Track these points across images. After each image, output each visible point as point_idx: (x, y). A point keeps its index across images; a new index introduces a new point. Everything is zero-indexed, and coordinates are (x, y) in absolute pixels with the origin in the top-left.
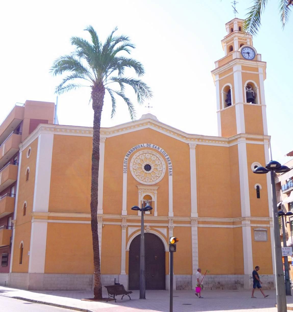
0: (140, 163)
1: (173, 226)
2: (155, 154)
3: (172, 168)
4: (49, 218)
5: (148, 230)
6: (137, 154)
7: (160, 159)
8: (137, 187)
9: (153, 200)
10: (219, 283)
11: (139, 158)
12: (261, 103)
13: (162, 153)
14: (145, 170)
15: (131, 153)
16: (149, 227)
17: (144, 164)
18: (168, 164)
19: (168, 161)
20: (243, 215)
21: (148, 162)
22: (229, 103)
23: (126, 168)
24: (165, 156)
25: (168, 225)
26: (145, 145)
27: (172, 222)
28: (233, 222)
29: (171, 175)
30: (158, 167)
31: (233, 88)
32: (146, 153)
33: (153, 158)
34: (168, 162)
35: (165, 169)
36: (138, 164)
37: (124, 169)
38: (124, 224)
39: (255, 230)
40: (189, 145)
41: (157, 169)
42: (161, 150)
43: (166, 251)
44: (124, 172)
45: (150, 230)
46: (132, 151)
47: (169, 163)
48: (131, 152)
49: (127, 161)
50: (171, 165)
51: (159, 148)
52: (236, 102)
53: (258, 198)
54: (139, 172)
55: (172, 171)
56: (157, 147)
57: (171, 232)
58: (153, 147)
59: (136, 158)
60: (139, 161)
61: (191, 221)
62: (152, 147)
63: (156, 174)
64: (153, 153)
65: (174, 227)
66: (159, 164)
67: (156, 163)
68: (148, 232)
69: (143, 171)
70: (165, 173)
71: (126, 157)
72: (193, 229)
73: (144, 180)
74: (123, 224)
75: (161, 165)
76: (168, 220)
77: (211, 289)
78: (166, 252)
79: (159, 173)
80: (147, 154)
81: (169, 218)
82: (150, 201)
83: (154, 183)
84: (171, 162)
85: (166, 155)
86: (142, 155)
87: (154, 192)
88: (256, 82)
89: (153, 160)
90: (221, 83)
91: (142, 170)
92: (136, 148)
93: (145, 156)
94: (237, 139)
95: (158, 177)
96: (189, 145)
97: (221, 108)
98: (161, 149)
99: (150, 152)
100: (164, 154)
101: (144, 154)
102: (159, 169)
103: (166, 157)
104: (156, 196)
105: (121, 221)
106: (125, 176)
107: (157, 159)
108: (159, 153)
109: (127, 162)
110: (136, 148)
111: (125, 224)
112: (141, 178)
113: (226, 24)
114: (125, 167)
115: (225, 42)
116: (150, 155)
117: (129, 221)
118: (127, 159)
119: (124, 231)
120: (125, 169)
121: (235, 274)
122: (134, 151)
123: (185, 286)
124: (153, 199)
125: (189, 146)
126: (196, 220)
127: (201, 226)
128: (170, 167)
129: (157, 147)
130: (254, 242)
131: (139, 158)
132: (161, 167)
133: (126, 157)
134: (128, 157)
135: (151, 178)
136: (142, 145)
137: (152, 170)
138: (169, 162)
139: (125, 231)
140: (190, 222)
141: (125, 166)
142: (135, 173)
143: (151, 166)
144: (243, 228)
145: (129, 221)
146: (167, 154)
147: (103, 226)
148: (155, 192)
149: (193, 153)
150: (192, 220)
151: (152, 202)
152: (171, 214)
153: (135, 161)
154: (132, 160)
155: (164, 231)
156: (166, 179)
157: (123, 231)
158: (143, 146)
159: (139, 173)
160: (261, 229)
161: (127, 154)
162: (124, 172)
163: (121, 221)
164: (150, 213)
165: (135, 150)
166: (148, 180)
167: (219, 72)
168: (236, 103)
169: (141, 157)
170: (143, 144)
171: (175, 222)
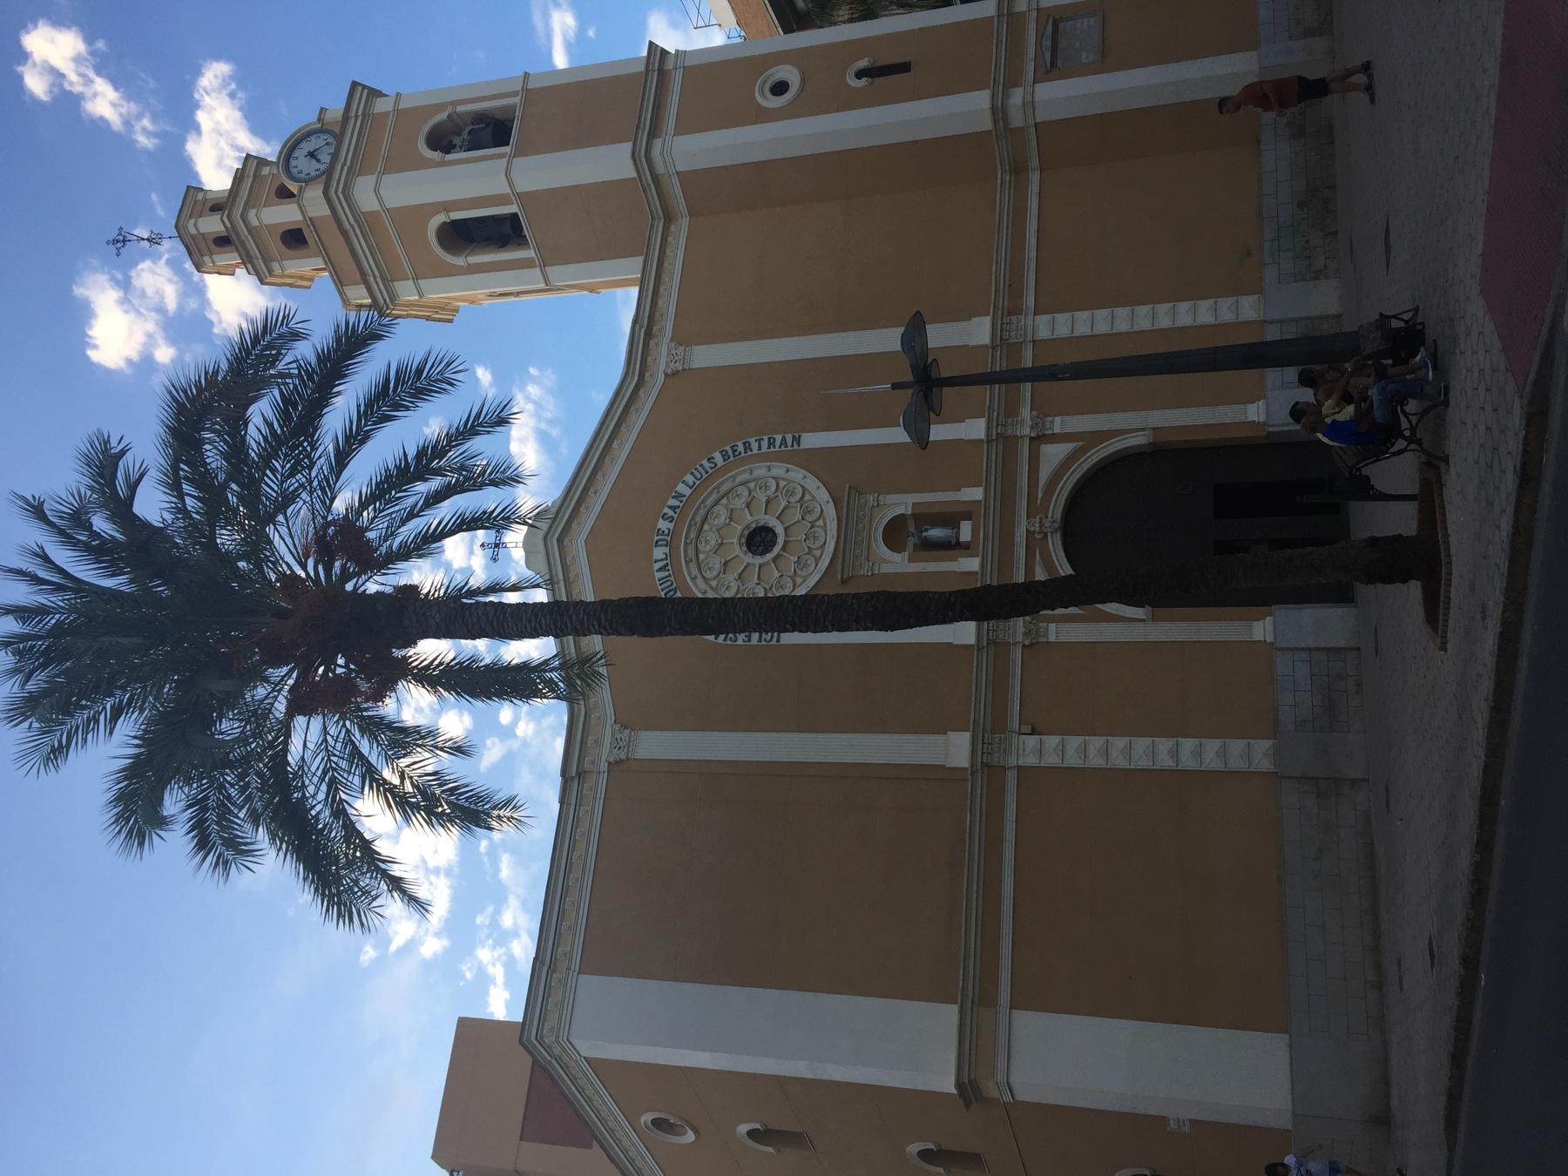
4: (987, 999)
10: (1301, 205)
12: (515, 94)
20: (986, 124)
22: (507, 229)
26: (659, 553)
29: (797, 440)
31: (446, 207)
39: (1053, 64)
41: (768, 502)
44: (774, 642)
50: (752, 440)
51: (678, 496)
53: (909, 70)
55: (779, 438)
57: (1058, 425)
62: (671, 526)
66: (746, 493)
73: (817, 553)
74: (1020, 638)
77: (1336, 233)
80: (708, 575)
82: (912, 528)
84: (740, 444)
93: (707, 553)
94: (656, 178)
98: (681, 488)
104: (890, 498)
107: (724, 501)
121: (1258, 142)
127: (1030, 301)
128: (765, 444)
130: (1105, 62)
136: (657, 566)
138: (741, 448)
139: (1052, 626)
144: (1041, 117)
146: (705, 462)
147: (1028, 729)
149: (706, 356)
155: (1053, 454)
156: (816, 462)
160: (1047, 43)
168: (377, 207)
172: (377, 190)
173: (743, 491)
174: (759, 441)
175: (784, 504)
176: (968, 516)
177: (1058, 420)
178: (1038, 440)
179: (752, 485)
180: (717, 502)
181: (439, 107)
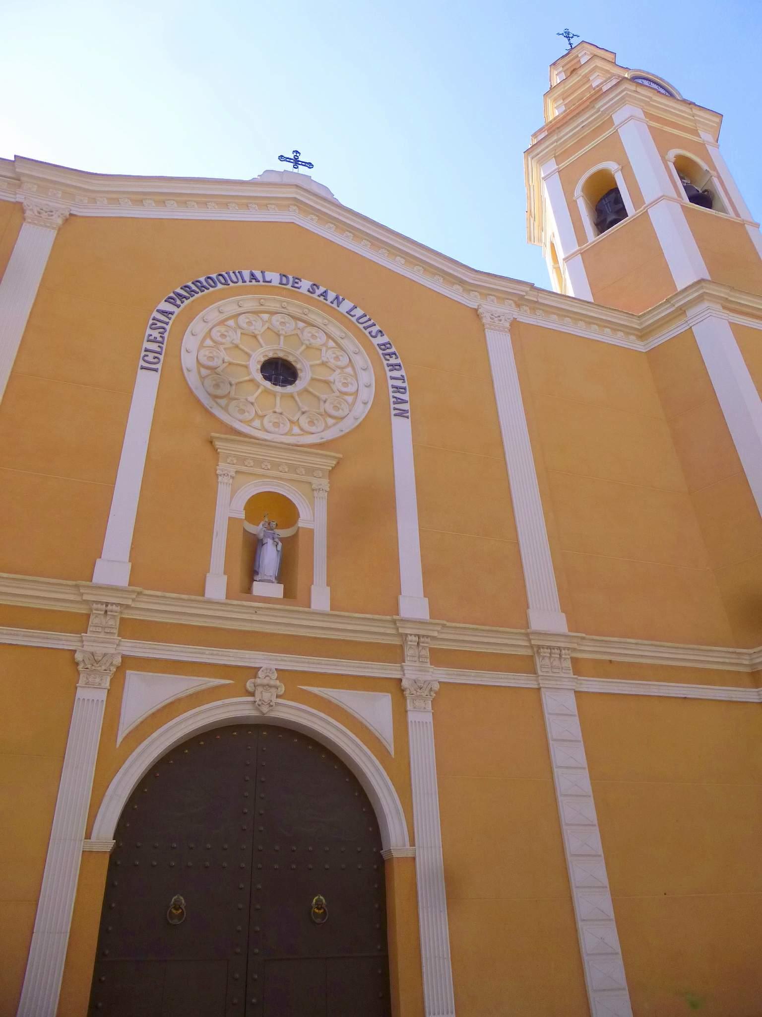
1: (429, 678)
2: (319, 321)
5: (266, 696)
7: (344, 343)
13: (354, 319)
14: (266, 378)
16: (276, 675)
19: (388, 357)
23: (159, 350)
25: (397, 675)
27: (426, 653)
28: (748, 670)
29: (402, 414)
31: (626, 168)
35: (368, 386)
36: (225, 349)
38: (99, 649)
42: (351, 310)
43: (395, 854)
44: (142, 363)
45: (280, 701)
47: (390, 362)
49: (167, 320)
52: (648, 198)
57: (421, 718)
58: (313, 293)
59: (222, 323)
60: (236, 338)
61: (531, 658)
63: (325, 402)
64: (312, 317)
65: (436, 687)
67: (324, 359)
68: (265, 709)
70: (369, 405)
72: (550, 701)
73: (257, 423)
74: (89, 647)
76: (397, 641)
78: (391, 859)
81: (401, 631)
85: (374, 329)
86: (251, 317)
87: (310, 483)
88: (703, 159)
90: (566, 178)
91: (249, 374)
94: (682, 311)
95: (330, 416)
97: (581, 238)
99: (292, 310)
102: (339, 386)
106: (146, 388)
107: (331, 344)
110: (223, 281)
111: (102, 644)
113: (554, 64)
115: (559, 96)
116: (296, 324)
119: (90, 698)
120: (151, 355)
126: (559, 648)
129: (331, 295)
132: (346, 375)
135: (295, 419)
137: (299, 385)
139: (103, 695)
140: (528, 665)
141: (155, 341)
145: (132, 628)
148: (315, 481)
149: (500, 349)
150: (539, 647)
151: (301, 539)
153: (215, 333)
155: (377, 711)
157: (82, 693)
159: (231, 385)
161: (172, 295)
164: (285, 595)
166: (276, 425)
167: (555, 149)
168: (647, 203)
170: (263, 272)
171: (439, 657)
172: (631, 117)
173: (344, 361)
174: (402, 378)
175: (323, 397)
176: (289, 594)
177: (428, 718)
178: (397, 687)
179: (349, 370)
180: (329, 336)
181: (708, 159)
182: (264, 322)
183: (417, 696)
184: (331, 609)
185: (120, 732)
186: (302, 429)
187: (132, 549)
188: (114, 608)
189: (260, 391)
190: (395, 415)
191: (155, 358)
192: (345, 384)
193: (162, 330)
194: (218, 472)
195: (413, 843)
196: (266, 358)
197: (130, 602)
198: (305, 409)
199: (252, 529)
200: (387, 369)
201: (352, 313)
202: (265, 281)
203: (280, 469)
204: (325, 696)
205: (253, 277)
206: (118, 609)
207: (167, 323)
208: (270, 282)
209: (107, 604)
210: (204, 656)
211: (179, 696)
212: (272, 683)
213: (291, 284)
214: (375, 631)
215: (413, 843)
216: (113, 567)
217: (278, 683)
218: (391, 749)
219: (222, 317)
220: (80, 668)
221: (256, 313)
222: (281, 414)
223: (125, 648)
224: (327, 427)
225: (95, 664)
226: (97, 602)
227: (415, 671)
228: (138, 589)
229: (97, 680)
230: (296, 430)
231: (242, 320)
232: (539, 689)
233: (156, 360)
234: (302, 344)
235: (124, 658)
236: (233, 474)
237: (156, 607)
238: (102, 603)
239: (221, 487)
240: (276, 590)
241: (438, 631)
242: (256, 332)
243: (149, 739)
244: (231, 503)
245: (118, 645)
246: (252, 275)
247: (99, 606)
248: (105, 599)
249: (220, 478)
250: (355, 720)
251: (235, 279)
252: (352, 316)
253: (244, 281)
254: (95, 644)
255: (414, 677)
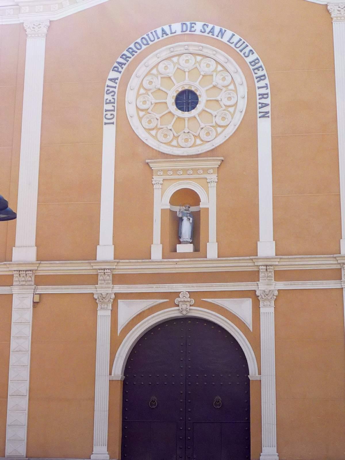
0: (156, 103)
1: (272, 288)
2: (210, 53)
3: (268, 91)
5: (184, 307)
6: (151, 60)
7: (229, 66)
8: (149, 165)
9: (202, 205)
11: (145, 89)
13: (233, 46)
15: (130, 60)
17: (174, 88)
18: (256, 80)
19: (256, 71)
21: (187, 81)
23: (112, 108)
24: (244, 54)
27: (273, 274)
29: (265, 115)
30: (222, 96)
32: (179, 55)
33: (187, 63)
34: (256, 73)
37: (106, 111)
38: (104, 291)
40: (329, 8)
41: (217, 101)
44: (105, 121)
45: (191, 308)
46: (133, 52)
48: (129, 55)
50: (267, 81)
51: (222, 33)
54: (158, 116)
55: (268, 101)
56: (217, 29)
58: (205, 32)
59: (149, 73)
60: (157, 83)
62: (198, 32)
64: (205, 52)
65: (276, 293)
66: (226, 83)
67: (214, 83)
69: (170, 112)
71: (113, 75)
73: (174, 143)
74: (100, 291)
75: (232, 87)
76: (256, 269)
79: (225, 114)
82: (193, 209)
83: (207, 147)
85: (247, 50)
89: (202, 73)
92: (145, 42)
96: (328, 11)
98: (228, 33)
99: (192, 49)
100: (241, 51)
101: (173, 56)
103: (248, 60)
105: (93, 279)
106: (109, 134)
107: (220, 68)
108: (226, 48)
109: (116, 90)
110: (145, 42)
112: (166, 136)
114: (109, 107)
117: (119, 279)
118: (117, 79)
119: (104, 315)
122: (139, 51)
123: (213, 181)
124: (201, 200)
125: (330, 14)
128: (263, 91)
129: (217, 29)
131: (145, 89)
132: (230, 95)
133: (113, 75)
134: (120, 72)
136: (167, 28)
138: (260, 73)
139: (109, 313)
141: (110, 102)
142: (145, 121)
143: (198, 93)
145: (119, 279)
146: (250, 48)
148: (208, 176)
152: (266, 247)
153: (146, 84)
154: (134, 82)
155: (243, 309)
156: (248, 130)
157: (100, 313)
158: (168, 32)
161: (116, 64)
162: (105, 121)
163: (93, 279)
165: (144, 47)
166: (186, 140)
169: (166, 68)
170: (170, 26)
171: (280, 275)
173: (229, 79)
175: (214, 113)
176: (196, 249)
182: (175, 64)
183: (266, 299)
184: (163, 258)
185: (118, 329)
186: (202, 140)
187: (113, 237)
188: (108, 271)
189: (175, 119)
190: (260, 117)
191: (111, 115)
192: (229, 99)
193: (113, 93)
194: (153, 182)
195: (260, 373)
196: (178, 93)
197: (114, 267)
198: (202, 125)
199: (176, 209)
200: (256, 80)
201: (231, 41)
202: (171, 33)
203: (188, 172)
204: (216, 303)
205: (164, 32)
206: (109, 271)
207: (115, 87)
208: (175, 33)
209: (104, 269)
210: (153, 289)
211: (143, 310)
212: (186, 300)
213: (189, 29)
214: (243, 265)
215: (260, 373)
216: (105, 251)
217: (189, 300)
218: (251, 328)
219: (148, 69)
220: (97, 301)
221: (169, 58)
222: (188, 133)
223: (116, 289)
224: (218, 135)
225: (103, 299)
226: (100, 269)
227: (265, 286)
228: (118, 261)
229: (106, 306)
230: (198, 142)
231: (161, 67)
232: (342, 288)
233: (112, 117)
234: (200, 74)
235: (115, 294)
236: (162, 182)
237: (127, 267)
238: (102, 269)
239: (155, 191)
240: (189, 248)
241: (278, 262)
242: (170, 75)
243: (131, 332)
244: (162, 201)
245: (113, 288)
246: (163, 30)
247: (101, 271)
248: (103, 267)
249: (155, 186)
250: (233, 314)
251: (152, 39)
252: (232, 43)
253: (158, 38)
254: (102, 289)
255: (263, 289)
